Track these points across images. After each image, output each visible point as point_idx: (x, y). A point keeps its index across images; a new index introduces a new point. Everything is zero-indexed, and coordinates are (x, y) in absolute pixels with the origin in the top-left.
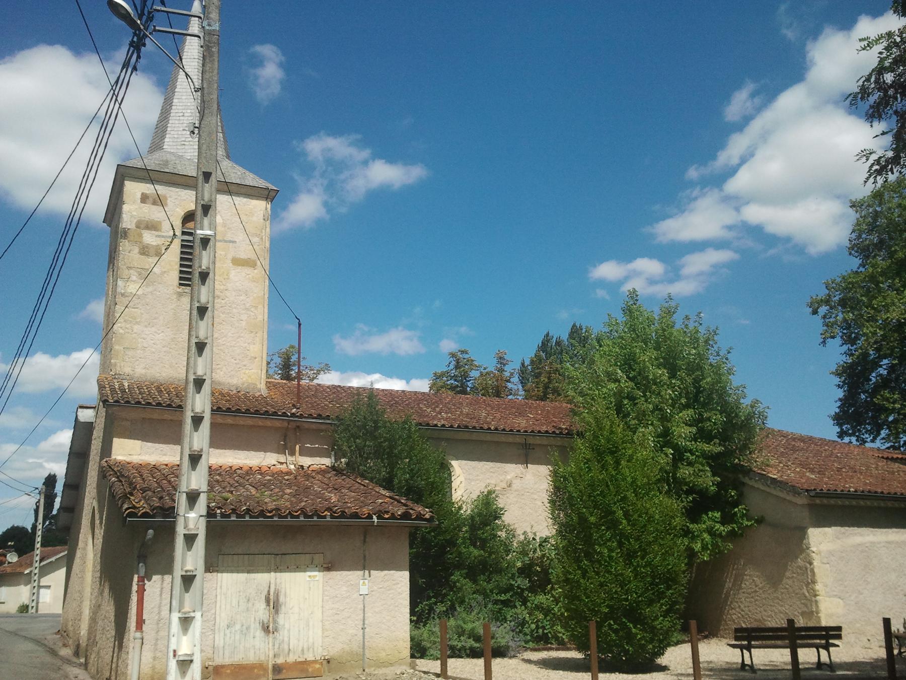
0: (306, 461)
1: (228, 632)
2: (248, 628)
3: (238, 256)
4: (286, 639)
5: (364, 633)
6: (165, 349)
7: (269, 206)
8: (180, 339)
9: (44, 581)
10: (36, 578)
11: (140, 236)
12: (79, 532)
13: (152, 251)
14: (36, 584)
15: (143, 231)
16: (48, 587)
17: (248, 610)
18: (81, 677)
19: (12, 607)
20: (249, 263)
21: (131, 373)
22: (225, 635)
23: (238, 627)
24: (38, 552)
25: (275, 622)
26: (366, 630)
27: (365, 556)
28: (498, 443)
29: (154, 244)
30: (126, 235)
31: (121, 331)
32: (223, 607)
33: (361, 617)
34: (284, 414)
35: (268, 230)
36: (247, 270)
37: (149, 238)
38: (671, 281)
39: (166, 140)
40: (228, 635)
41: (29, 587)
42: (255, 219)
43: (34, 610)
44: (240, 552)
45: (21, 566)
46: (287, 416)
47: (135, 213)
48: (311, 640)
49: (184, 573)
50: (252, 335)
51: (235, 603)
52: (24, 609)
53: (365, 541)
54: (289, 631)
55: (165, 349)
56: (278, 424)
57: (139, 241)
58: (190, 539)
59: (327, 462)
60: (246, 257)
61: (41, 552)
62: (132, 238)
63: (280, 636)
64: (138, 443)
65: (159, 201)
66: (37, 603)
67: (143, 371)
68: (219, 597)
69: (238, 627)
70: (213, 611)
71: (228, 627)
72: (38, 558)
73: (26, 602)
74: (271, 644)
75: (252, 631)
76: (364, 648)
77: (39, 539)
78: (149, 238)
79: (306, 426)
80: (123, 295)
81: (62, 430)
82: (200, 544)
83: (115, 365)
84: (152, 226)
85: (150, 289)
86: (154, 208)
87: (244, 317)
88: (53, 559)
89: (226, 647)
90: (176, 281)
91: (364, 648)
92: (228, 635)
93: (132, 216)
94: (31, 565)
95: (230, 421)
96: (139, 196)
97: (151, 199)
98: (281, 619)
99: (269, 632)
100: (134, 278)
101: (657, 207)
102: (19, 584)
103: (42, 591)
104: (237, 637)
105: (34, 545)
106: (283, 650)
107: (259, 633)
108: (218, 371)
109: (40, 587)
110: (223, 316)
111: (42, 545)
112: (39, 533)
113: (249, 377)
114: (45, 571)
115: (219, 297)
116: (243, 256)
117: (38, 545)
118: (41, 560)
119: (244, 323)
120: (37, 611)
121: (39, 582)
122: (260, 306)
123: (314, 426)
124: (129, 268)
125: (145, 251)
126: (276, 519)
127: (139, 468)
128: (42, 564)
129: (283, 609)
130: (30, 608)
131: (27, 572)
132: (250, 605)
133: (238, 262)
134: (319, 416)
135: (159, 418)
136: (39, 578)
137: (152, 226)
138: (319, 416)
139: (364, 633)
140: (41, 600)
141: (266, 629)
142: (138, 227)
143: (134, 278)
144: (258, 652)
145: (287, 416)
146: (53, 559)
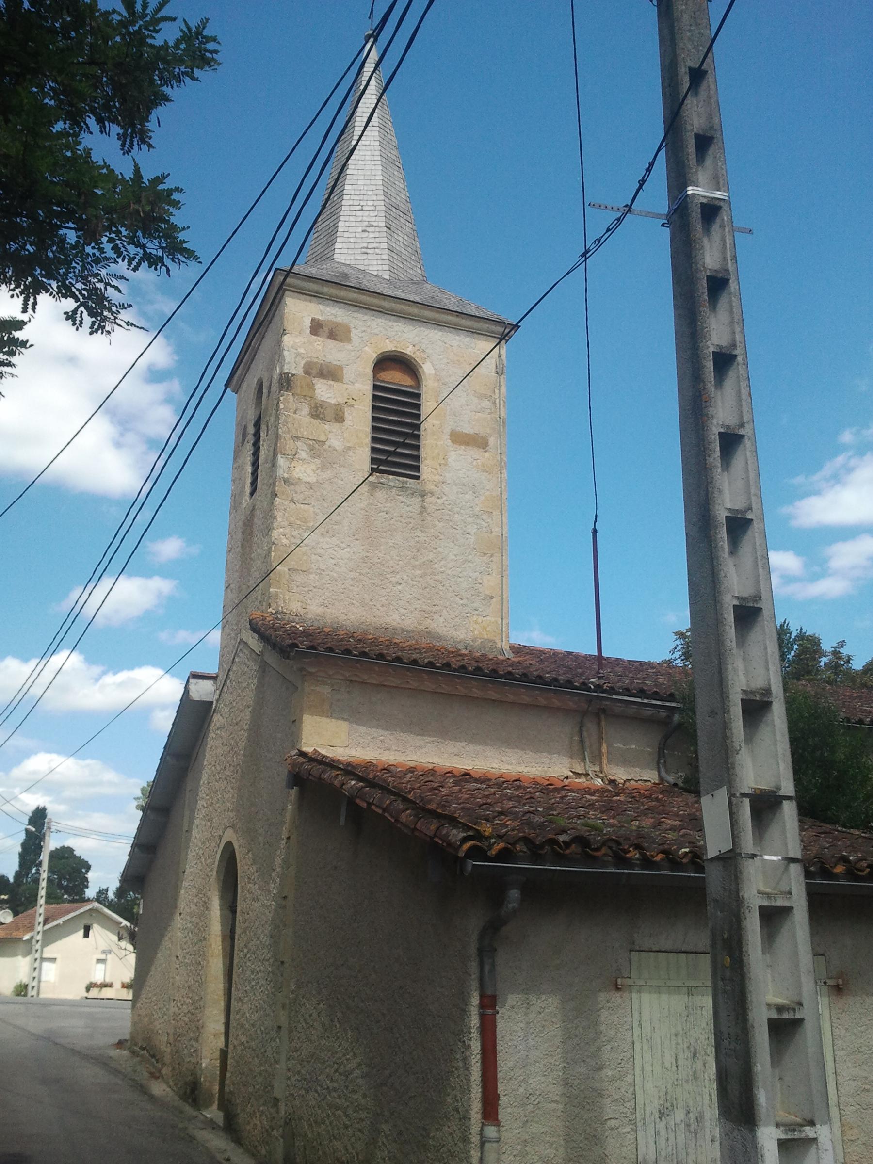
0: (620, 774)
1: (661, 1126)
2: (699, 1119)
3: (459, 429)
6: (353, 575)
8: (376, 560)
9: (48, 952)
10: (38, 946)
11: (311, 387)
12: (177, 888)
14: (37, 955)
15: (315, 381)
16: (53, 960)
18: (234, 1159)
19: (7, 988)
20: (478, 442)
21: (302, 611)
22: (657, 1133)
23: (679, 1115)
24: (41, 910)
30: (289, 384)
31: (285, 541)
32: (648, 1068)
34: (585, 686)
35: (503, 389)
36: (473, 452)
37: (325, 391)
38: (814, 578)
39: (337, 246)
40: (663, 1132)
41: (28, 959)
43: (34, 993)
44: (668, 946)
45: (17, 929)
46: (589, 689)
47: (302, 351)
49: (775, 1016)
51: (669, 1060)
52: (22, 990)
55: (353, 575)
57: (309, 396)
58: (773, 917)
59: (651, 776)
60: (472, 432)
61: (45, 910)
62: (298, 390)
64: (344, 725)
65: (336, 333)
66: (39, 982)
67: (320, 610)
68: (638, 1046)
69: (679, 1115)
70: (629, 1079)
71: (662, 1115)
72: (41, 919)
73: (25, 980)
77: (42, 893)
78: (325, 391)
79: (618, 709)
80: (286, 481)
81: (36, 753)
82: (44, 898)
83: (277, 595)
84: (330, 373)
85: (329, 474)
86: (331, 343)
87: (472, 529)
88: (60, 921)
90: (367, 466)
92: (663, 1132)
93: (298, 355)
94: (31, 928)
96: (308, 323)
97: (326, 329)
100: (303, 455)
101: (799, 480)
102: (14, 955)
103: (46, 965)
104: (681, 1139)
105: (36, 900)
108: (436, 616)
109: (43, 959)
110: (440, 525)
111: (46, 902)
112: (44, 884)
114: (50, 937)
115: (432, 494)
117: (42, 901)
118: (46, 921)
119: (472, 539)
120: (38, 993)
121: (42, 952)
122: (496, 513)
124: (296, 438)
125: (318, 412)
127: (350, 770)
128: (47, 927)
130: (30, 988)
131: (26, 937)
133: (460, 439)
134: (642, 693)
136: (43, 946)
138: (642, 693)
140: (43, 978)
142: (307, 372)
143: (303, 455)
145: (589, 689)
146: (60, 921)
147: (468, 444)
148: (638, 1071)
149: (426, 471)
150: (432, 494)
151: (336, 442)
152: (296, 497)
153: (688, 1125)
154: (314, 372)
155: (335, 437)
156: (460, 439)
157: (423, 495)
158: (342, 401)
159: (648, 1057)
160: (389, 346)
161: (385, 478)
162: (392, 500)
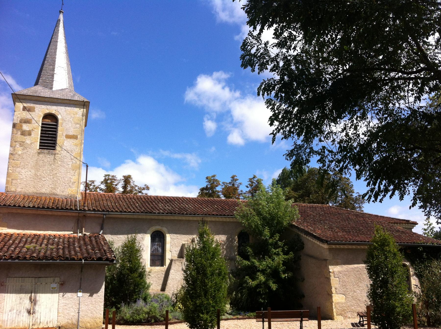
1: (10, 313)
2: (20, 312)
4: (39, 317)
5: (79, 315)
7: (85, 110)
11: (21, 126)
13: (27, 133)
17: (20, 303)
20: (74, 137)
22: (8, 315)
23: (15, 311)
25: (34, 309)
26: (80, 314)
27: (81, 279)
28: (189, 221)
29: (28, 130)
32: (8, 302)
33: (78, 307)
37: (26, 127)
42: (78, 116)
44: (26, 276)
48: (51, 318)
50: (74, 171)
53: (82, 271)
54: (40, 313)
56: (74, 214)
62: (17, 127)
63: (36, 315)
71: (10, 311)
74: (31, 319)
75: (22, 313)
76: (78, 322)
79: (89, 215)
84: (27, 121)
89: (9, 321)
91: (78, 322)
95: (50, 213)
98: (37, 308)
99: (30, 314)
104: (14, 316)
106: (37, 322)
107: (26, 314)
113: (72, 191)
116: (71, 134)
119: (70, 166)
123: (98, 215)
126: (58, 261)
129: (38, 303)
132: (21, 301)
133: (68, 137)
135: (16, 212)
137: (27, 121)
139: (79, 315)
141: (29, 312)
142: (20, 122)
144: (24, 323)
147: (70, 138)
148: (5, 302)
149: (58, 148)
150: (58, 154)
151: (28, 142)
152: (15, 158)
153: (16, 313)
154: (23, 122)
155: (28, 140)
156: (68, 137)
157: (55, 154)
158: (31, 129)
159: (8, 299)
160: (47, 112)
161: (43, 151)
162: (47, 157)
